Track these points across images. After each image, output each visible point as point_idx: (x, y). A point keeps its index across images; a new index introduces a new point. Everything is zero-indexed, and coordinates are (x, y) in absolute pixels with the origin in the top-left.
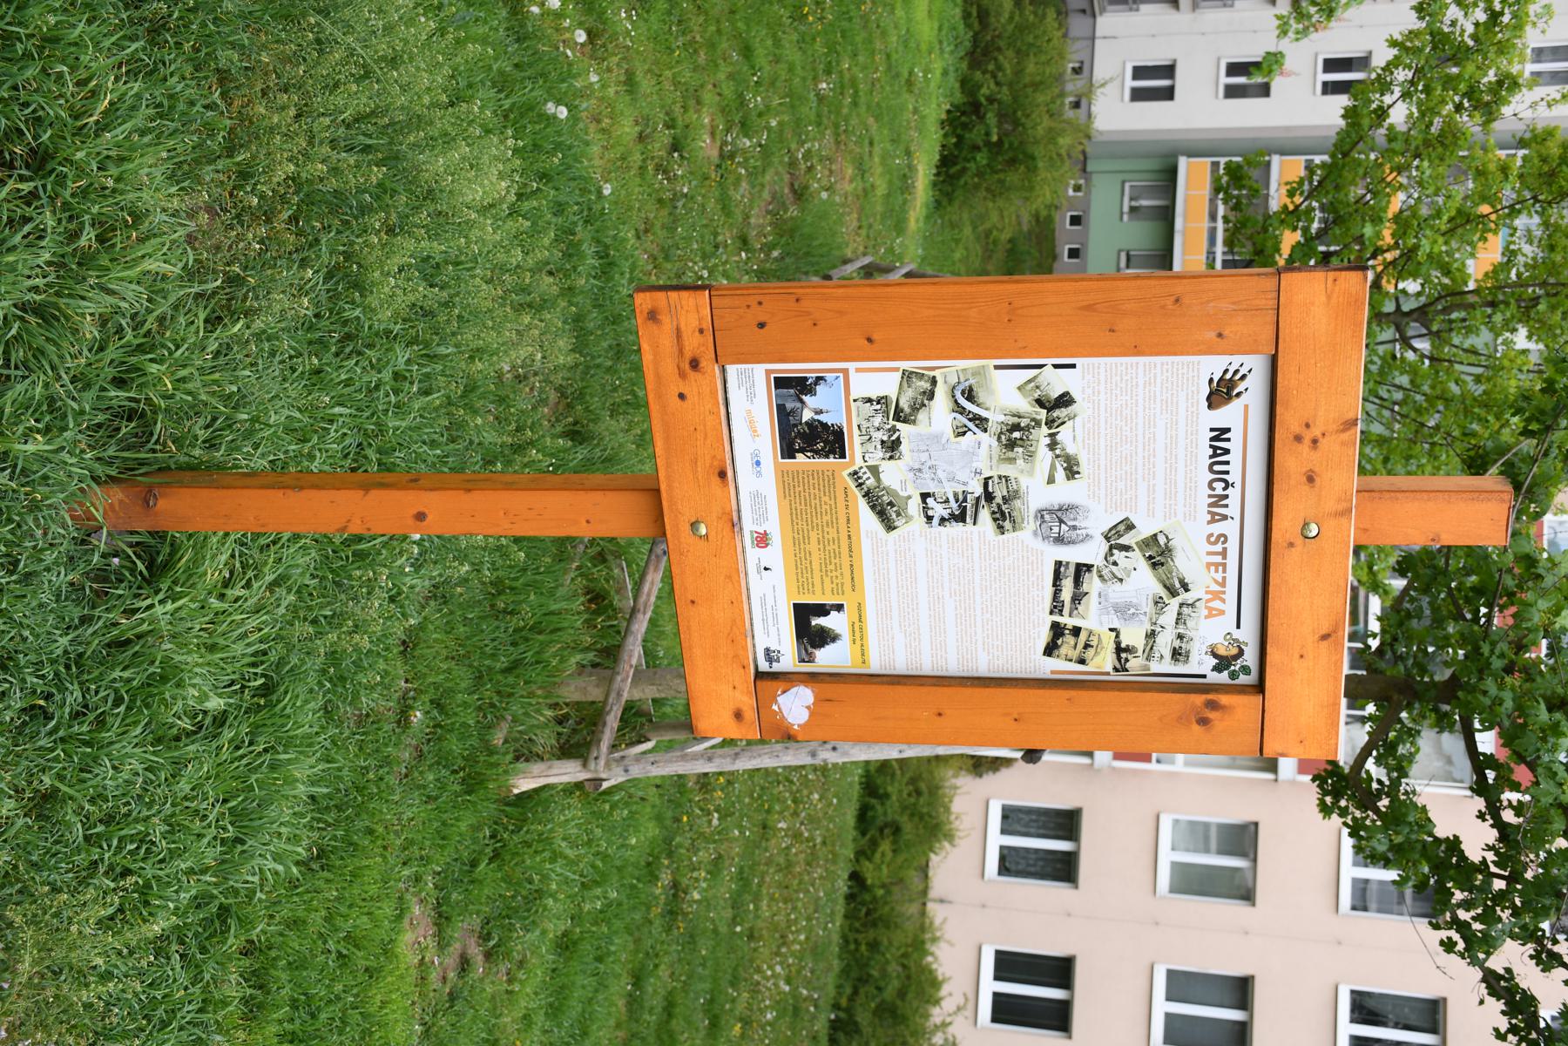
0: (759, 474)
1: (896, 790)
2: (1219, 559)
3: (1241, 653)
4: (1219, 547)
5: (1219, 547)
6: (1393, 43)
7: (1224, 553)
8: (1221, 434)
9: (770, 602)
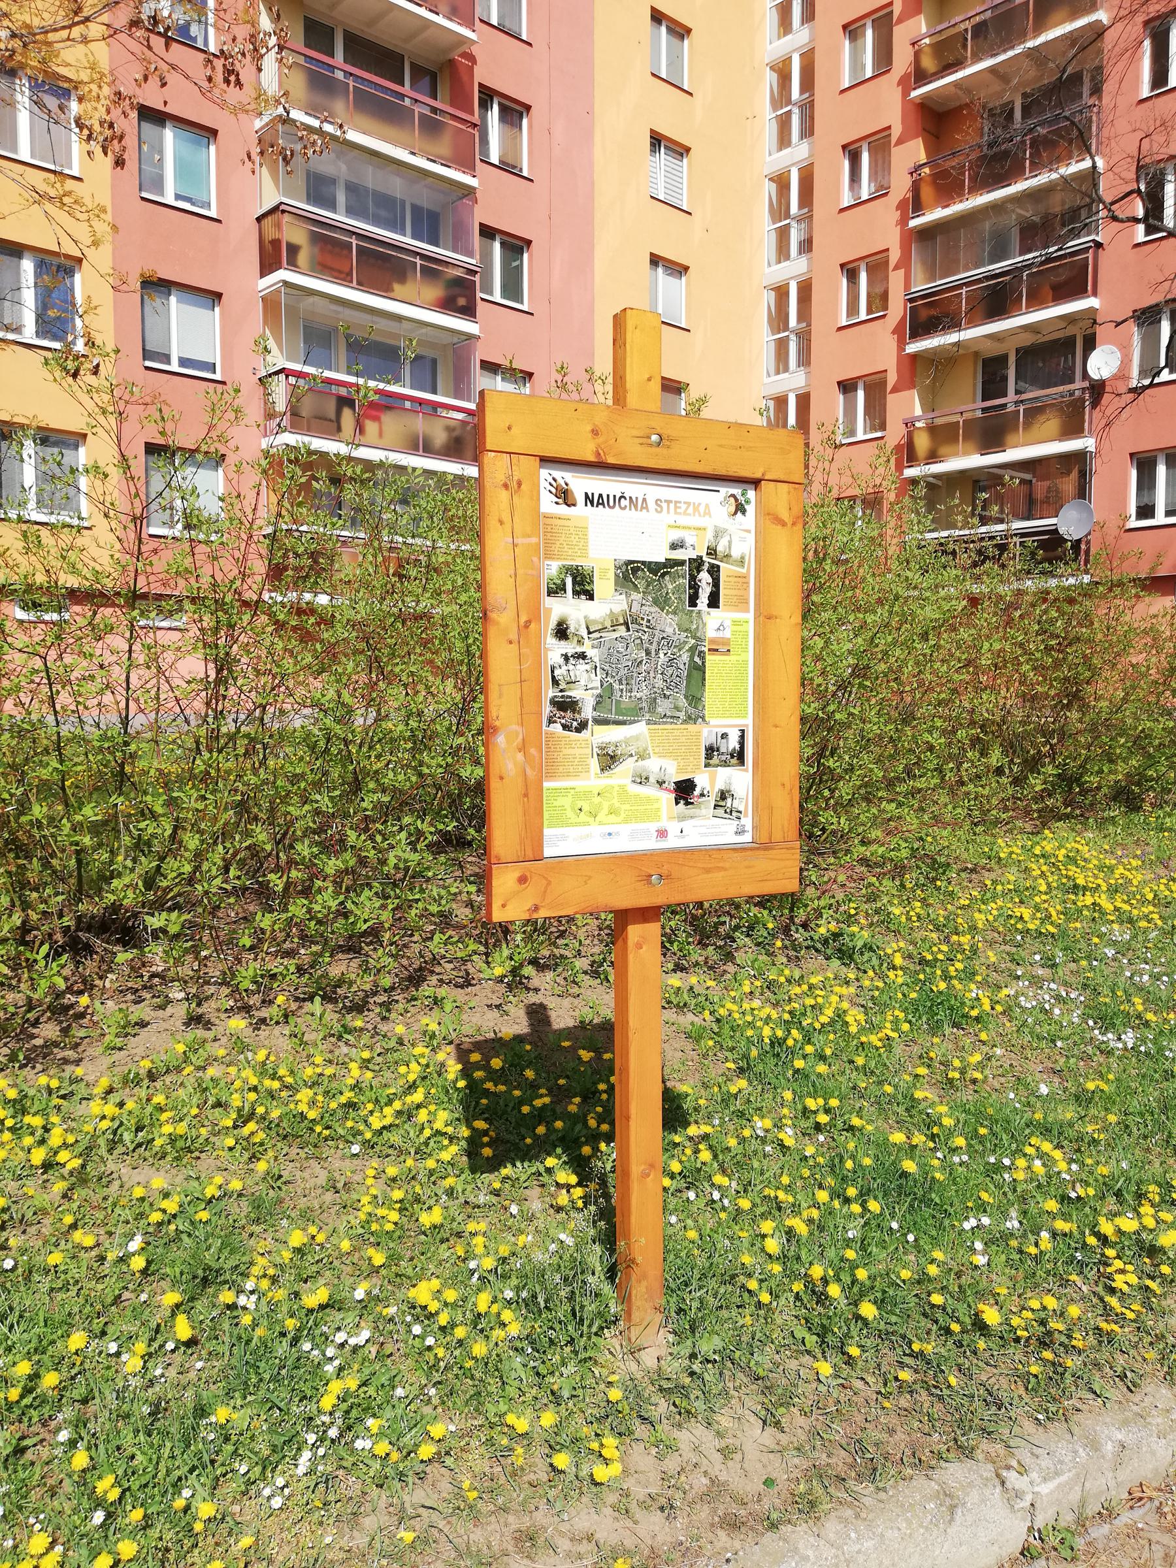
0: (618, 833)
1: (345, 252)
2: (672, 506)
3: (733, 496)
4: (664, 505)
5: (664, 505)
6: (677, 803)
7: (668, 502)
8: (589, 499)
9: (703, 830)
